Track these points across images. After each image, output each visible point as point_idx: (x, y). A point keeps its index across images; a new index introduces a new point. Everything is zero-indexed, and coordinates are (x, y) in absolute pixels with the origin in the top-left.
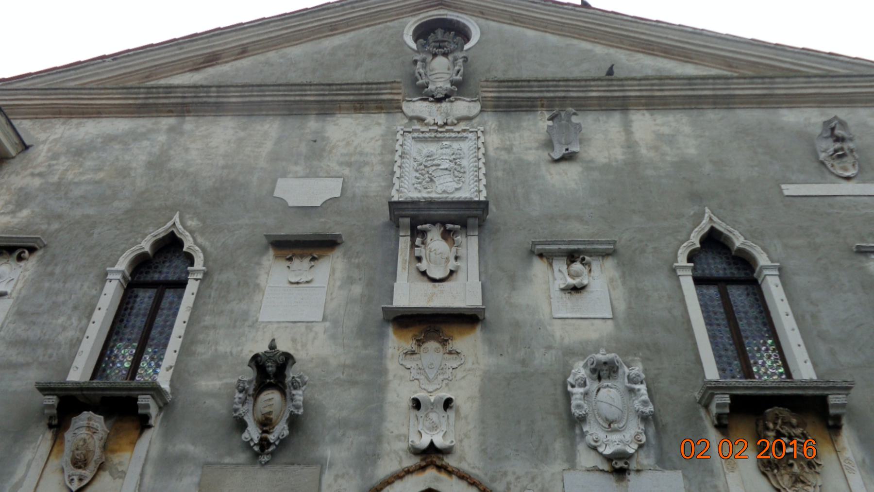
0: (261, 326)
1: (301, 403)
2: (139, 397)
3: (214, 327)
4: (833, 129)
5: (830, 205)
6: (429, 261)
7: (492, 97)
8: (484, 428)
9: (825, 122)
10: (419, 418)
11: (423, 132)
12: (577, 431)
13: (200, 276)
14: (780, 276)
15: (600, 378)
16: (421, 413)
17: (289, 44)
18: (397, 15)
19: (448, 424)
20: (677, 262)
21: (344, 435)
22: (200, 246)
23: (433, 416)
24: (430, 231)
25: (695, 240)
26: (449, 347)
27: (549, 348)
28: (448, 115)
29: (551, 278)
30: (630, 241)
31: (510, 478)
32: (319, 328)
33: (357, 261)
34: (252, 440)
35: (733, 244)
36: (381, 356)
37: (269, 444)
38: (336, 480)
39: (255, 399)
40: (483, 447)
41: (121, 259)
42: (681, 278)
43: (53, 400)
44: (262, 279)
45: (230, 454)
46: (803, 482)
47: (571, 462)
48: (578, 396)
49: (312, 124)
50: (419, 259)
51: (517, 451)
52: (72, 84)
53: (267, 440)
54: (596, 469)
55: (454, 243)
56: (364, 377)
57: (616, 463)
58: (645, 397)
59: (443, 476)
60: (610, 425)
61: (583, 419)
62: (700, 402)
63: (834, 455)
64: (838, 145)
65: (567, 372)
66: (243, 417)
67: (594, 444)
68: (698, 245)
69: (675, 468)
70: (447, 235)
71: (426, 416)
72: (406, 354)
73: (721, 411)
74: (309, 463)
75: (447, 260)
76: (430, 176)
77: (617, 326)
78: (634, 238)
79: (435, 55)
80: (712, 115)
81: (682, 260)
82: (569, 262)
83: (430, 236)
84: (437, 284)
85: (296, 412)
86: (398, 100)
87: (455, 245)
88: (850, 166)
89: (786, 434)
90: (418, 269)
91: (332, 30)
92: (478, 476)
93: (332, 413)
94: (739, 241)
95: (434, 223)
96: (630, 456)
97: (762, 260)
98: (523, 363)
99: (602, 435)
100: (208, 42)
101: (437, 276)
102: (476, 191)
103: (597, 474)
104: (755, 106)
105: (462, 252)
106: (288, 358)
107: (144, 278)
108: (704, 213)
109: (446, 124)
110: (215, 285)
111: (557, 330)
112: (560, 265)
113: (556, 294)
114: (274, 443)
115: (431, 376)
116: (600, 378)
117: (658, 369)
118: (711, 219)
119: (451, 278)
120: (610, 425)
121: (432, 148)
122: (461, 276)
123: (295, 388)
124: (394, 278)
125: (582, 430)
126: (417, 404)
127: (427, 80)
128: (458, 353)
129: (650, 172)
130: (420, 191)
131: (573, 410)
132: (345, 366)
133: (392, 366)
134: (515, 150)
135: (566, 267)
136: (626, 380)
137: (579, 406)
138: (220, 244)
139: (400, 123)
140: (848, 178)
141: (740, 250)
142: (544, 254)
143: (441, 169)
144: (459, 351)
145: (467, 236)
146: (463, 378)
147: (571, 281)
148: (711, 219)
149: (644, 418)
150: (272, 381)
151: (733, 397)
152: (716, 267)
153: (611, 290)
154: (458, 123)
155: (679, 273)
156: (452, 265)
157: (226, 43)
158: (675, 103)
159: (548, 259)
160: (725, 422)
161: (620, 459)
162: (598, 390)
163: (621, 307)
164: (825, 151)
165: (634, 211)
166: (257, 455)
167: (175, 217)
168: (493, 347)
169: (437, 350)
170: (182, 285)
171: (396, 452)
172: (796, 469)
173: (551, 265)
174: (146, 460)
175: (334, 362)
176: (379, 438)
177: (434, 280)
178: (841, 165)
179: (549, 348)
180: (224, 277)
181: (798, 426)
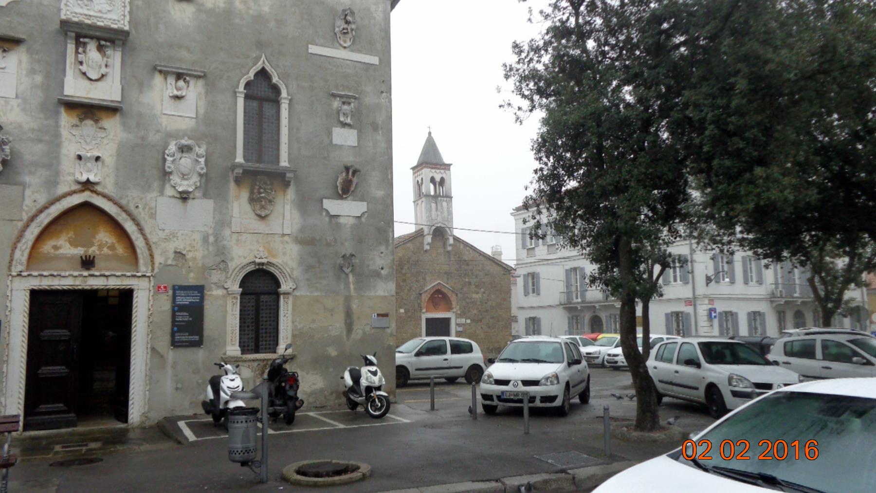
1: (9, 153)
4: (346, 15)
5: (329, 63)
6: (88, 65)
12: (167, 178)
14: (289, 104)
15: (182, 152)
16: (82, 162)
19: (98, 169)
20: (238, 88)
21: (36, 170)
23: (89, 165)
25: (251, 75)
26: (100, 125)
27: (158, 131)
29: (165, 88)
32: (14, 103)
33: (37, 57)
36: (57, 125)
42: (238, 98)
47: (162, 192)
48: (169, 162)
50: (81, 63)
54: (174, 197)
56: (47, 138)
58: (203, 166)
59: (94, 195)
61: (171, 173)
62: (230, 168)
63: (283, 197)
64: (346, 26)
65: (166, 147)
67: (174, 185)
68: (252, 78)
69: (211, 198)
70: (100, 48)
71: (85, 164)
72: (73, 126)
73: (237, 175)
74: (16, 184)
75: (100, 67)
77: (197, 123)
81: (241, 88)
83: (89, 47)
84: (93, 82)
85: (6, 158)
88: (348, 40)
93: (28, 157)
94: (275, 79)
96: (190, 192)
97: (284, 94)
98: (143, 138)
101: (93, 78)
102: (122, 15)
105: (110, 61)
111: (164, 121)
112: (171, 80)
113: (166, 98)
115: (88, 141)
116: (182, 152)
118: (264, 62)
120: (184, 176)
122: (109, 79)
123: (4, 145)
124: (65, 75)
125: (169, 177)
126: (80, 157)
128: (105, 129)
129: (237, 21)
130: (82, 7)
131: (166, 168)
133: (65, 132)
135: (174, 82)
136: (195, 155)
137: (169, 167)
140: (345, 48)
144: (106, 127)
145: (114, 50)
146: (108, 144)
147: (176, 93)
148: (264, 62)
149: (201, 175)
152: (263, 90)
155: (238, 95)
156: (104, 70)
159: (164, 75)
162: (181, 158)
163: (202, 111)
164: (339, 27)
168: (126, 127)
169: (92, 126)
171: (67, 181)
172: (263, 203)
173: (166, 78)
175: (26, 126)
176: (57, 173)
177: (91, 80)
178: (344, 39)
179: (158, 131)
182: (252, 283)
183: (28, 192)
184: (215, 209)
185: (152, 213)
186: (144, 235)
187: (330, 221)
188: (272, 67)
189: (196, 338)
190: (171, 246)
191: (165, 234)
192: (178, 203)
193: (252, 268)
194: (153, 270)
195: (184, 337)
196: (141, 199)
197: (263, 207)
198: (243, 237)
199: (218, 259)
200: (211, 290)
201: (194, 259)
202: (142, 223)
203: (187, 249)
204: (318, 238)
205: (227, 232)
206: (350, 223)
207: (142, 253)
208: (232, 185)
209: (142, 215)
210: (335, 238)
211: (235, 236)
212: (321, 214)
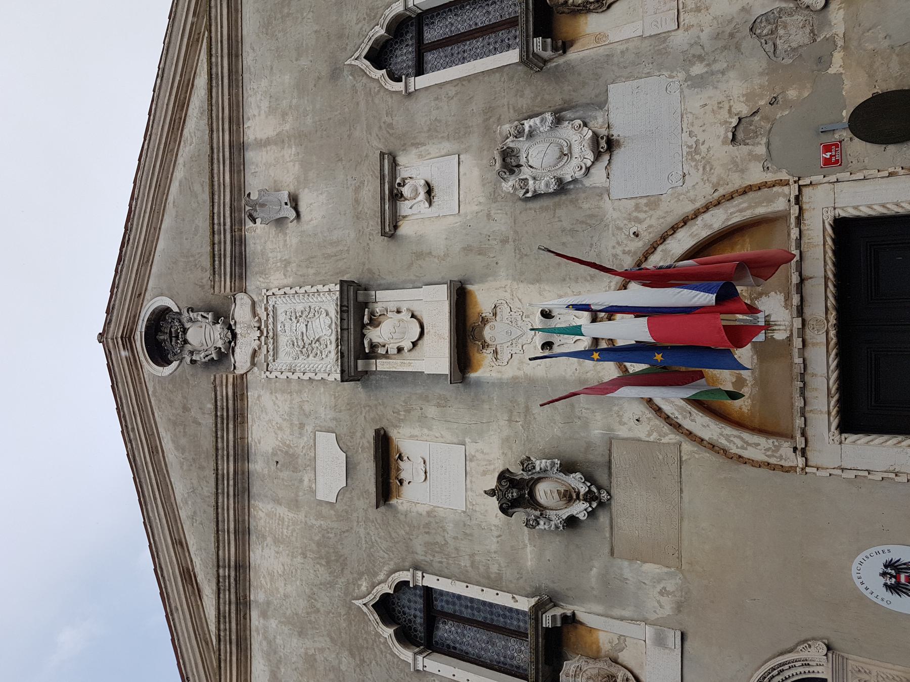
0: (471, 507)
2: (544, 626)
3: (472, 556)
10: (561, 343)
13: (419, 574)
15: (519, 166)
17: (172, 496)
18: (141, 383)
22: (388, 576)
24: (371, 340)
27: (489, 216)
28: (249, 327)
30: (380, 139)
31: (618, 251)
32: (472, 448)
33: (402, 413)
34: (586, 510)
35: (381, 36)
36: (500, 384)
37: (590, 491)
38: (625, 424)
39: (546, 508)
40: (589, 278)
44: (423, 509)
49: (257, 466)
53: (586, 494)
55: (384, 314)
57: (602, 148)
60: (565, 155)
66: (563, 520)
70: (374, 322)
72: (496, 359)
73: (549, 48)
76: (313, 343)
77: (466, 151)
78: (377, 135)
79: (186, 342)
80: (249, 58)
82: (403, 199)
83: (376, 340)
87: (386, 313)
90: (410, 351)
91: (158, 452)
95: (363, 336)
99: (575, 162)
100: (170, 581)
104: (240, 15)
106: (504, 476)
108: (350, 65)
110: (429, 558)
111: (470, 208)
114: (589, 487)
115: (519, 333)
117: (508, 108)
119: (419, 317)
121: (283, 340)
127: (213, 349)
132: (510, 420)
134: (286, 257)
138: (386, 555)
139: (257, 376)
141: (387, 31)
142: (394, 224)
143: (307, 331)
150: (526, 492)
151: (536, 35)
153: (431, 156)
156: (405, 316)
158: (237, 94)
160: (560, 43)
161: (598, 143)
163: (447, 146)
165: (349, 136)
166: (601, 504)
167: (358, 604)
170: (428, 591)
175: (506, 432)
179: (489, 216)
180: (420, 549)
183: (623, 432)
184: (628, 78)
185: (646, 205)
186: (696, 214)
191: (693, 171)
192: (620, 155)
194: (787, 183)
196: (619, 229)
202: (671, 220)
207: (741, 211)
208: (573, 55)
211: (686, 18)
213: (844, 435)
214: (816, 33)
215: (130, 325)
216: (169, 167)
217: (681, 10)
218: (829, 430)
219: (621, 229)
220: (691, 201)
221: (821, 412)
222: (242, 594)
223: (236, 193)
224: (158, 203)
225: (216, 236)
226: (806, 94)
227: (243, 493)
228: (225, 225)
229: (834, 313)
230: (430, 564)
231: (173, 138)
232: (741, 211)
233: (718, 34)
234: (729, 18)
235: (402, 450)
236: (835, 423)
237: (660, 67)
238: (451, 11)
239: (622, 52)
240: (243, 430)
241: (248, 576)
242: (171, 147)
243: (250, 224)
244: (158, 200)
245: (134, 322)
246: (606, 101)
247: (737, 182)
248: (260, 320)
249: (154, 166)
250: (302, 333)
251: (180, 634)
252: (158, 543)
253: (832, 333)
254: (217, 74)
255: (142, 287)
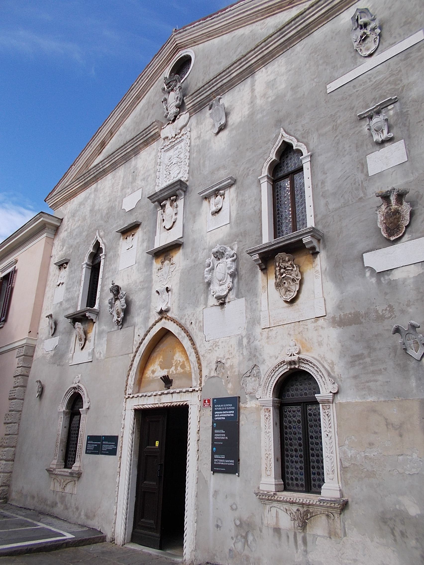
2: (303, 239)
7: (191, 107)
8: (180, 297)
9: (352, 18)
11: (174, 141)
18: (162, 70)
31: (187, 317)
41: (263, 170)
43: (257, 257)
45: (113, 327)
46: (289, 291)
51: (189, 304)
52: (67, 184)
86: (157, 132)
89: (283, 267)
92: (176, 318)
98: (195, 260)
103: (214, 307)
104: (325, 22)
107: (281, 174)
109: (176, 135)
151: (259, 254)
154: (181, 131)
157: (104, 134)
158: (278, 52)
163: (234, 215)
170: (301, 169)
174: (95, 334)
181: (289, 261)
182: (297, 390)
183: (136, 330)
184: (246, 307)
185: (200, 326)
186: (195, 349)
187: (379, 282)
188: (290, 135)
189: (231, 462)
190: (213, 357)
191: (210, 344)
193: (285, 369)
194: (200, 385)
195: (221, 460)
197: (287, 290)
198: (273, 333)
199: (251, 364)
200: (246, 402)
201: (232, 367)
203: (227, 357)
204: (363, 312)
205: (258, 330)
206: (412, 276)
207: (194, 368)
209: (194, 330)
210: (390, 306)
212: (364, 275)
213: (133, 411)
214: (251, 395)
215: (183, 45)
216: (250, 21)
217: (269, 329)
218: (135, 406)
219: (193, 316)
220: (200, 346)
221: (138, 403)
222: (98, 177)
223: (229, 84)
224: (233, 25)
225: (207, 85)
226: (228, 392)
227: (126, 159)
228: (213, 87)
229: (162, 406)
230: (107, 261)
231: (263, 13)
232: (194, 368)
233: (256, 349)
234: (262, 354)
235: (135, 235)
236: (136, 407)
237: (248, 323)
238: (278, 199)
239: (257, 302)
240: (143, 147)
241: (271, 60)
242: (259, 15)
243: (208, 107)
244: (234, 25)
245: (185, 47)
246: (239, 298)
247: (204, 364)
248: (179, 133)
249: (247, 11)
250: (172, 163)
251: (85, 153)
252: (108, 123)
253: (157, 406)
254: (126, 147)
255: (198, 41)
